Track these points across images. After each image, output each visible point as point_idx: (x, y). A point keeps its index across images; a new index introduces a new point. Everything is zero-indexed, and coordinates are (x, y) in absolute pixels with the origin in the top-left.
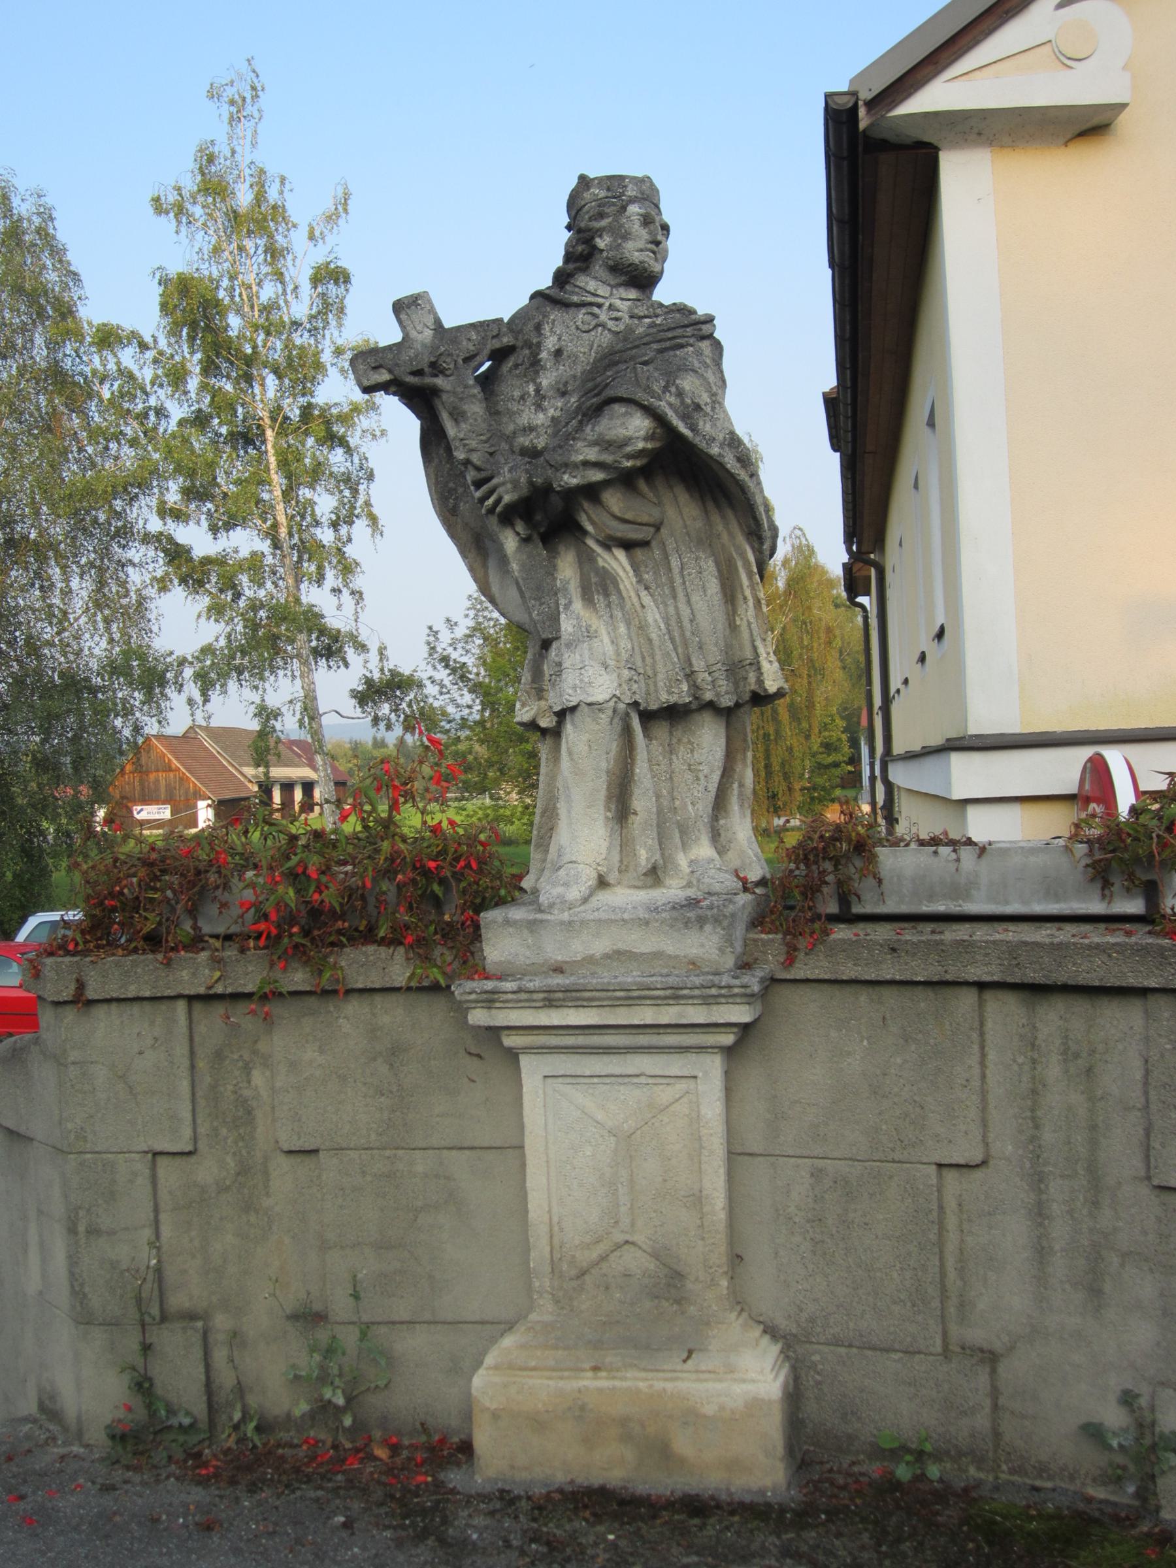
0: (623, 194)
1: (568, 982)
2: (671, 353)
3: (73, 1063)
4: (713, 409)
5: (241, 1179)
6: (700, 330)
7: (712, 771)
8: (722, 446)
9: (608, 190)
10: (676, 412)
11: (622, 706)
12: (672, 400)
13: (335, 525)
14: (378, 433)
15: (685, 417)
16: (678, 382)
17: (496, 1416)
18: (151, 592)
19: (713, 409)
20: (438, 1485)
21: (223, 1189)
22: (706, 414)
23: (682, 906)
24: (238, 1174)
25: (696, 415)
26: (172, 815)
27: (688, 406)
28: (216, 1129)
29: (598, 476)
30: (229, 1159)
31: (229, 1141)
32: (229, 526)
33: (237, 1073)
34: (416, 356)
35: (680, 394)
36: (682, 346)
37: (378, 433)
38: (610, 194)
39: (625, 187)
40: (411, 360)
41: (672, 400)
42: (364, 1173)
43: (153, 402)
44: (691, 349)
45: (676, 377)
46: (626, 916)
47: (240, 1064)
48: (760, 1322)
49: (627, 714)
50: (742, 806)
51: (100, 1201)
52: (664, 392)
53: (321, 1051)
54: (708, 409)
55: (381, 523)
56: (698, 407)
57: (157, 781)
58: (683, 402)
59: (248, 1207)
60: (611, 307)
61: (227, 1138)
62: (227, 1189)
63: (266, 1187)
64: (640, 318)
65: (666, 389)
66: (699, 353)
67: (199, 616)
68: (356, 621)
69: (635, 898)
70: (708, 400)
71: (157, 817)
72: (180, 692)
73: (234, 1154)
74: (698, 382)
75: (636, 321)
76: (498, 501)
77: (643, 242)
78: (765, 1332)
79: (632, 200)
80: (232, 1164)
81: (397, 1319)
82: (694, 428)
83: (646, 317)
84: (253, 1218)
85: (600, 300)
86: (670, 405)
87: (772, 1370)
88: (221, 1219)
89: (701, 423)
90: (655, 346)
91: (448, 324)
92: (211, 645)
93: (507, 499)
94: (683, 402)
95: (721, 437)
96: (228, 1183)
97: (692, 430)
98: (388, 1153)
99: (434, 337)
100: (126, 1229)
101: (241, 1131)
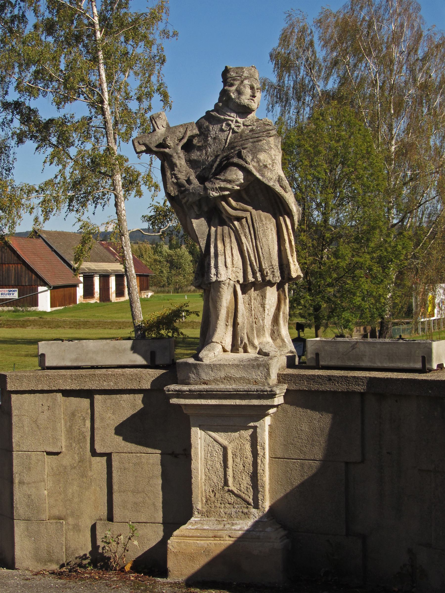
0: (242, 75)
1: (207, 387)
2: (257, 143)
3: (15, 415)
4: (273, 166)
5: (80, 464)
6: (269, 133)
7: (271, 307)
8: (274, 182)
9: (237, 73)
10: (256, 169)
11: (232, 282)
12: (255, 164)
13: (139, 99)
14: (171, 34)
15: (259, 171)
16: (258, 156)
17: (176, 554)
18: (12, 143)
19: (273, 166)
20: (155, 580)
21: (73, 468)
22: (269, 169)
23: (252, 360)
24: (79, 462)
25: (264, 170)
26: (19, 296)
27: (261, 167)
28: (71, 444)
29: (227, 193)
30: (76, 456)
31: (76, 448)
32: (66, 99)
33: (80, 421)
34: (158, 139)
35: (258, 162)
36: (261, 141)
37: (171, 34)
38: (237, 75)
39: (244, 72)
40: (156, 141)
41: (255, 164)
42: (129, 463)
43: (16, 12)
44: (265, 141)
45: (257, 155)
46: (230, 363)
47: (82, 418)
48: (280, 524)
49: (235, 285)
50: (284, 321)
51: (25, 471)
52: (251, 161)
53: (113, 413)
54: (270, 166)
55: (170, 100)
56: (265, 166)
57: (8, 269)
58: (259, 165)
59: (83, 475)
60: (237, 122)
61: (75, 447)
62: (75, 468)
63: (90, 467)
64: (247, 126)
65: (252, 160)
66: (268, 143)
67: (45, 162)
68: (150, 165)
69: (235, 356)
70: (271, 163)
71: (8, 297)
72: (31, 213)
73: (78, 454)
74: (266, 156)
75: (246, 127)
76: (188, 201)
77: (249, 96)
78: (281, 527)
79: (246, 78)
80: (77, 458)
81: (141, 521)
82: (263, 175)
83: (250, 126)
84: (85, 480)
85: (232, 118)
86: (254, 166)
87: (280, 538)
88: (72, 479)
89: (266, 173)
90: (251, 140)
91: (171, 126)
92: (52, 181)
93: (190, 200)
94: (259, 165)
95: (274, 178)
96: (75, 465)
97: (262, 176)
98: (138, 455)
99: (166, 131)
100: (35, 482)
101: (81, 445)
